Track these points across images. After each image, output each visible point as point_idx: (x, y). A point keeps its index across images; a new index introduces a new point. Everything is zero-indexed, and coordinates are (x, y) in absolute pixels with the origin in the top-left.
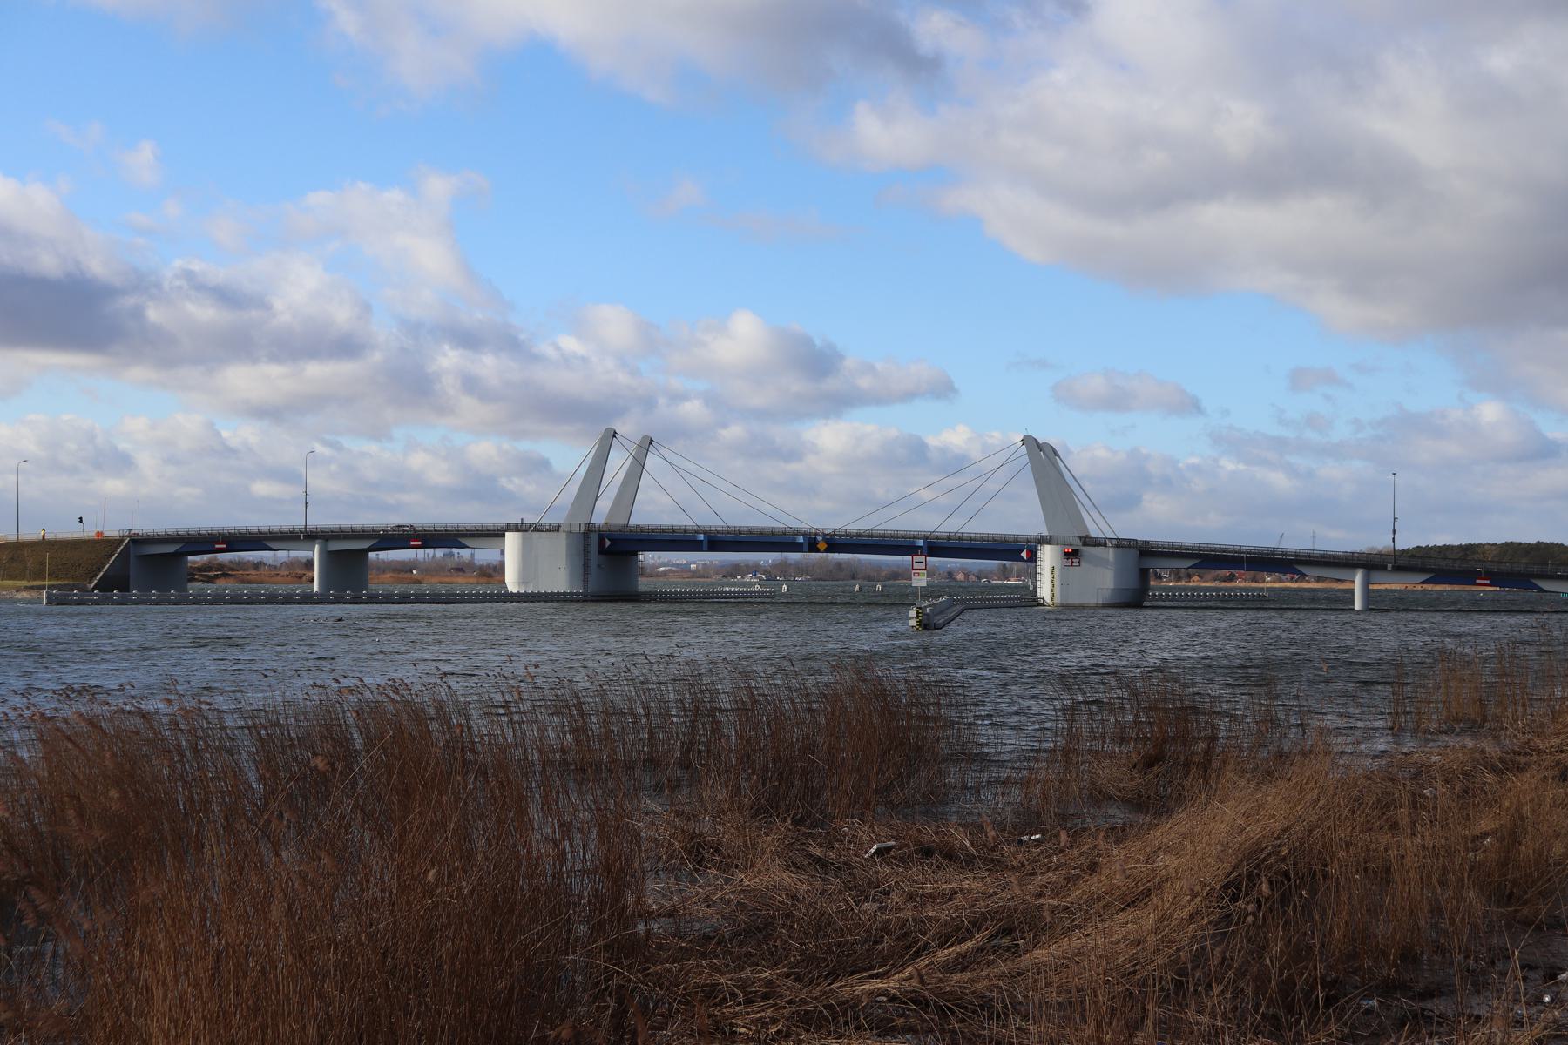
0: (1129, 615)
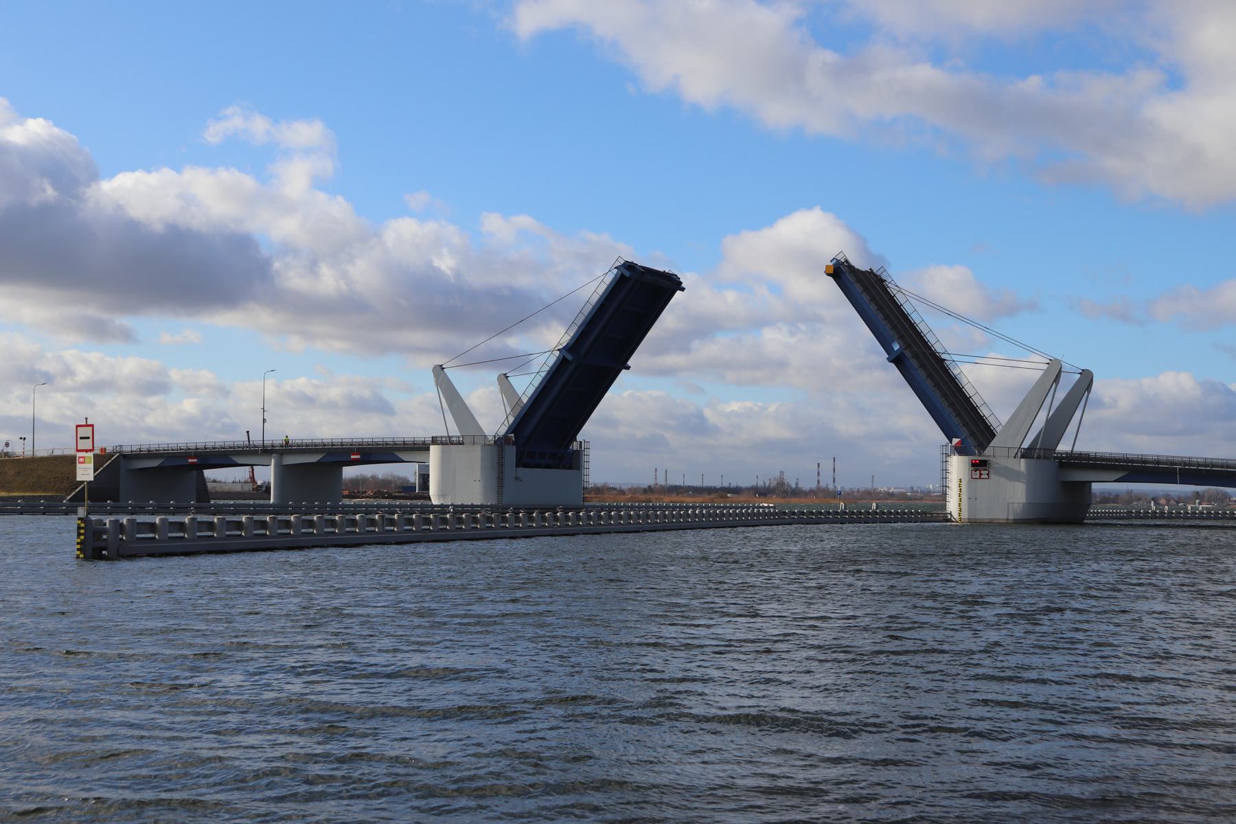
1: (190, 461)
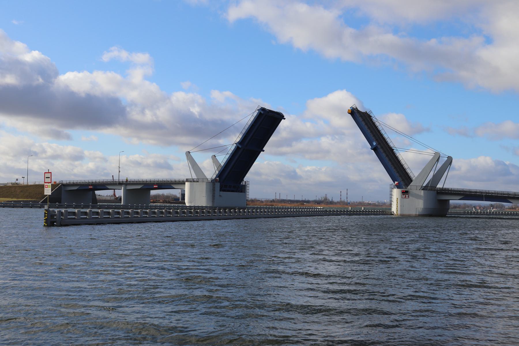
0: (431, 222)
1: (89, 187)
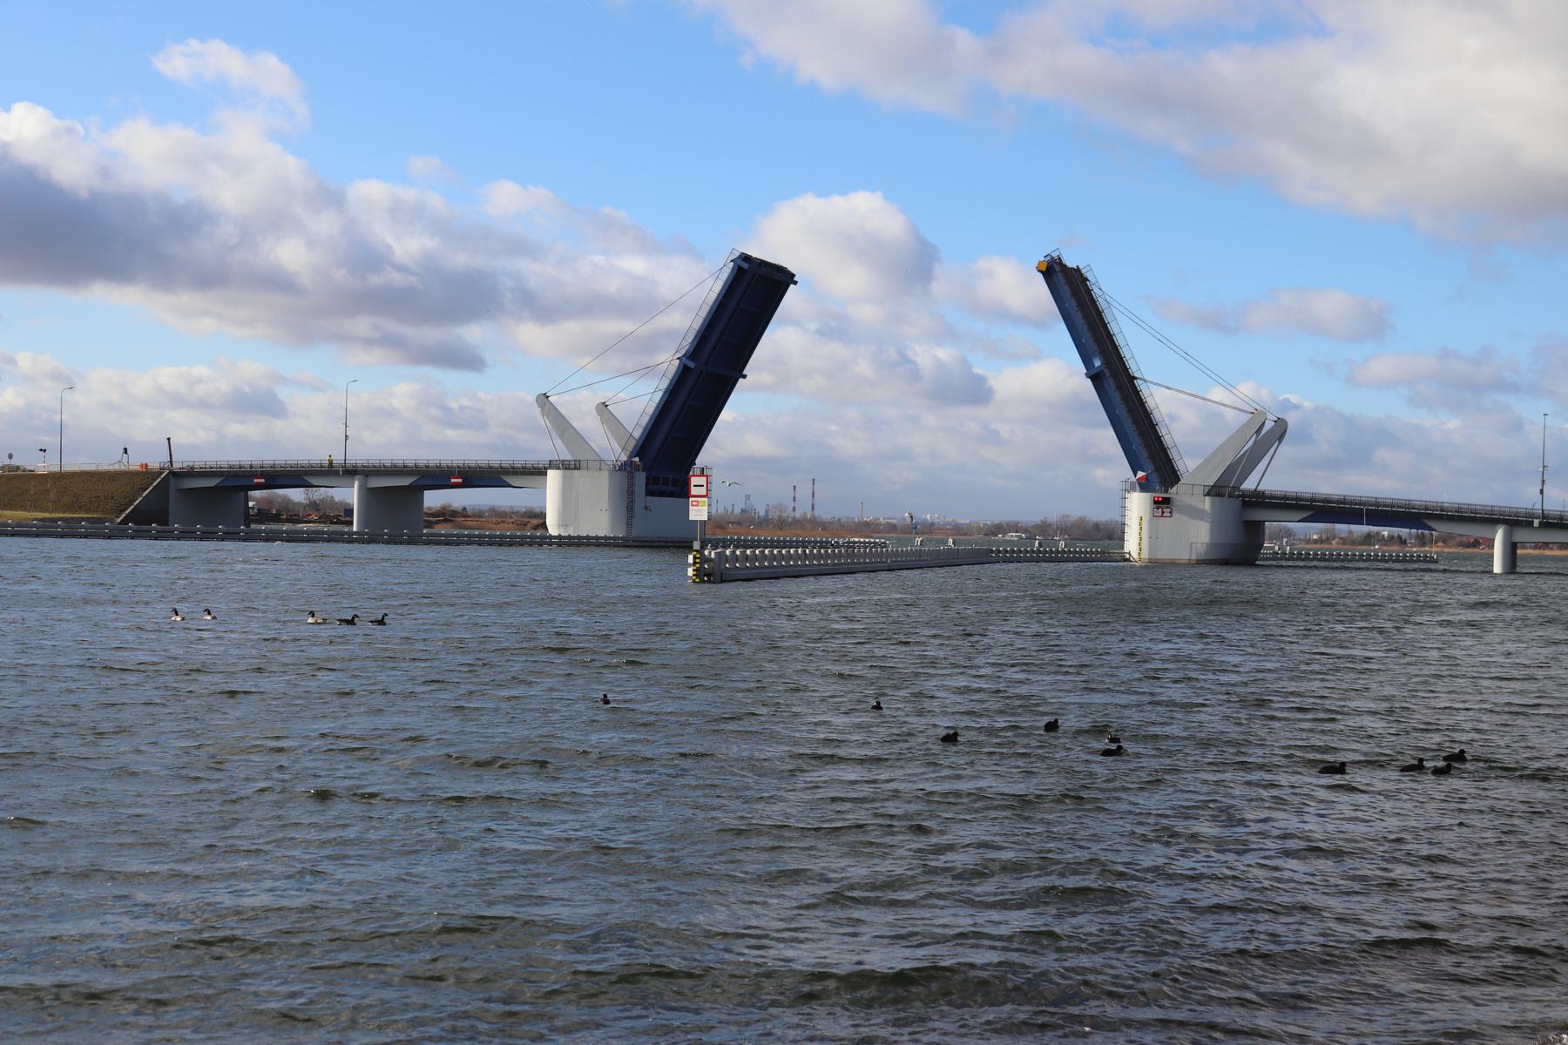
1: (256, 481)
